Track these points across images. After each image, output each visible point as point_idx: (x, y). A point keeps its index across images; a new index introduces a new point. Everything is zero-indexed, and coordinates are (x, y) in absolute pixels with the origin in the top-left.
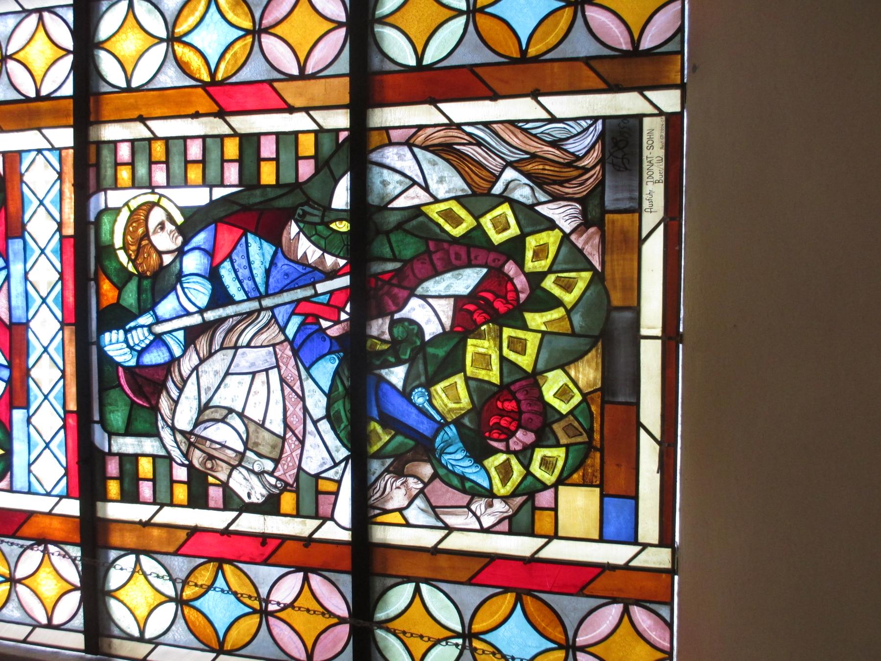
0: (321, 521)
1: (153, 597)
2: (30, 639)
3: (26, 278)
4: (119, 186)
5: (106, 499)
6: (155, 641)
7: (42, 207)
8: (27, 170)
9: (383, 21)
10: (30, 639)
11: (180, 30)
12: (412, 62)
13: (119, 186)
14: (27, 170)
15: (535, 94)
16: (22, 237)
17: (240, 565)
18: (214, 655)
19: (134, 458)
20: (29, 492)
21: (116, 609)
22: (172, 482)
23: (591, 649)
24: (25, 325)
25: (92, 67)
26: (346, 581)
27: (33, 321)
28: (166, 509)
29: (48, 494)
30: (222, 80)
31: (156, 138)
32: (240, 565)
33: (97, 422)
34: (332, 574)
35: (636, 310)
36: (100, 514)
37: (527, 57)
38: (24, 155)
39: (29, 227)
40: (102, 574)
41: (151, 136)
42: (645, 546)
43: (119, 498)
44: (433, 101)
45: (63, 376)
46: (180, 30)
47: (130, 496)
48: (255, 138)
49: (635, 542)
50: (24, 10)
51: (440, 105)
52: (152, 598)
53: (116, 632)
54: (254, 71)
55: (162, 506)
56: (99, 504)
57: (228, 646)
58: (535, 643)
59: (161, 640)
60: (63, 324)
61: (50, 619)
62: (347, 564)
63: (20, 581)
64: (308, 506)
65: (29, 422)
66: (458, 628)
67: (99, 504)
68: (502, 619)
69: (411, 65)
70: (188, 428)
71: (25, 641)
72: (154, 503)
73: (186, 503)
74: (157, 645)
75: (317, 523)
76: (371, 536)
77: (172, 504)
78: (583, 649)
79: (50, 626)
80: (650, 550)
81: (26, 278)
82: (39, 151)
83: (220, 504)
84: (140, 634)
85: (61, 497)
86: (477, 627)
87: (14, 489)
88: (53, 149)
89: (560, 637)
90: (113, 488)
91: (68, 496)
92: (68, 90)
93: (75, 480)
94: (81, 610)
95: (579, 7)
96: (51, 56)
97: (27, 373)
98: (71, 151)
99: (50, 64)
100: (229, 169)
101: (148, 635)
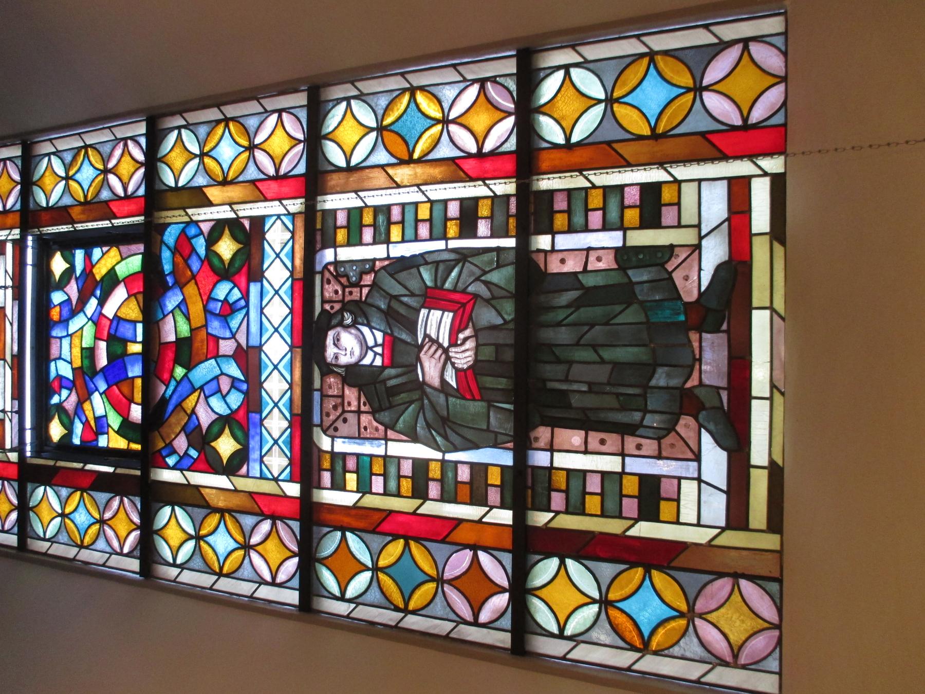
0: (361, 494)
1: (217, 543)
2: (214, 587)
3: (262, 313)
4: (419, 239)
5: (320, 487)
6: (355, 601)
7: (278, 259)
10: (214, 587)
11: (246, 154)
13: (419, 239)
16: (261, 282)
17: (287, 521)
18: (217, 577)
22: (567, 491)
24: (259, 348)
25: (320, 153)
26: (507, 558)
27: (266, 345)
31: (594, 187)
32: (287, 521)
33: (317, 426)
34: (364, 534)
39: (266, 274)
41: (590, 185)
43: (410, 495)
46: (246, 154)
47: (339, 485)
50: (117, 139)
52: (182, 536)
53: (31, 534)
54: (697, 123)
56: (315, 491)
59: (186, 566)
60: (292, 347)
61: (274, 577)
62: (508, 544)
67: (315, 491)
68: (631, 591)
70: (10, 410)
71: (104, 565)
72: (357, 491)
73: (499, 505)
77: (371, 493)
79: (273, 583)
81: (262, 313)
82: (279, 216)
84: (474, 619)
86: (611, 596)
87: (681, 521)
90: (326, 477)
92: (141, 192)
93: (298, 470)
94: (298, 573)
97: (260, 385)
100: (562, 225)
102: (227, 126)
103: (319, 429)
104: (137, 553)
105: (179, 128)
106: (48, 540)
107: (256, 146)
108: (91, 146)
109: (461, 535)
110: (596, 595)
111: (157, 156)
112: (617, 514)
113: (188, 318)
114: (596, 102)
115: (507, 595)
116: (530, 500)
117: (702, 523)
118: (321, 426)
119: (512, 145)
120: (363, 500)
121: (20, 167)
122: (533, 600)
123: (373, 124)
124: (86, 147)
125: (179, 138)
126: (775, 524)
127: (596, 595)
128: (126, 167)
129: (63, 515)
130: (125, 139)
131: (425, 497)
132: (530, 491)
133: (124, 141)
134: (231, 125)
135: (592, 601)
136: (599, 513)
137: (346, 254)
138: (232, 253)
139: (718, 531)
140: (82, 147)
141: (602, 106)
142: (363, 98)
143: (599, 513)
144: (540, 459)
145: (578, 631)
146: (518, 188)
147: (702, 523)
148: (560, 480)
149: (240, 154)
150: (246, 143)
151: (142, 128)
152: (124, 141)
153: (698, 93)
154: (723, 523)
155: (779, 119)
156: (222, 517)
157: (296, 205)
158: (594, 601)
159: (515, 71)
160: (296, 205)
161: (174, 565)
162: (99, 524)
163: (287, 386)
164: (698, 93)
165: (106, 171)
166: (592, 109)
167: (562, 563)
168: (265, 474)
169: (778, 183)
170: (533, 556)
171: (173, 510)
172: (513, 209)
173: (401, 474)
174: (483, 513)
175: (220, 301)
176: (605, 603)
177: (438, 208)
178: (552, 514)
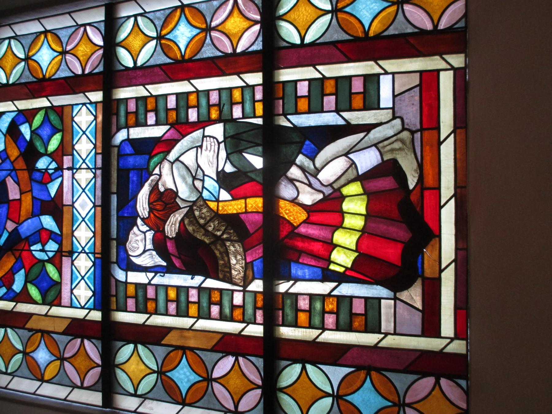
2: (68, 398)
8: (76, 115)
9: (281, 18)
10: (68, 398)
12: (298, 41)
14: (76, 115)
15: (238, 74)
19: (377, 301)
20: (71, 307)
21: (121, 376)
23: (415, 406)
26: (260, 362)
27: (76, 203)
28: (250, 325)
29: (83, 308)
30: (188, 59)
35: (438, 188)
36: (277, 335)
37: (305, 43)
38: (74, 107)
40: (114, 355)
42: (386, 334)
44: (188, 79)
45: (94, 236)
48: (125, 101)
49: (380, 332)
50: (77, 25)
51: (192, 81)
54: (63, 73)
55: (248, 324)
57: (46, 378)
58: (380, 402)
63: (66, 359)
64: (317, 321)
65: (72, 264)
66: (156, 369)
69: (297, 43)
74: (14, 376)
75: (147, 316)
76: (275, 332)
78: (410, 405)
80: (389, 336)
82: (84, 104)
83: (174, 313)
85: (90, 310)
88: (91, 103)
89: (205, 375)
91: (95, 309)
95: (208, 32)
96: (357, 5)
98: (261, 88)
99: (16, 64)
101: (139, 393)
102: (46, 37)
103: (116, 265)
104: (100, 385)
105: (10, 38)
106: (10, 374)
107: (68, 52)
108: (49, 31)
109: (170, 339)
110: (155, 368)
111: (275, 14)
112: (294, 324)
113: (18, 183)
114: (99, 48)
115: (259, 392)
116: (281, 319)
117: (397, 332)
118: (117, 263)
119: (258, 46)
120: (89, 315)
121: (103, 32)
122: (282, 397)
123: (154, 34)
124: (46, 32)
125: (136, 25)
126: (460, 334)
127: (155, 368)
128: (83, 50)
129: (62, 359)
130: (85, 25)
131: (324, 329)
132: (114, 299)
133: (84, 27)
134: (187, 11)
135: (119, 366)
136: (134, 310)
137: (137, 133)
138: (203, 120)
139: (449, 340)
140: (41, 33)
141: (329, 16)
142: (147, 15)
143: (134, 310)
144: (283, 287)
145: (144, 393)
146: (104, 96)
147: (397, 332)
148: (131, 290)
149: (95, 52)
150: (60, 49)
151: (99, 16)
152: (84, 27)
153: (400, 6)
154: (452, 335)
155: (462, 24)
156: (184, 353)
157: (97, 96)
158: (154, 372)
159: (103, 19)
160: (97, 96)
161: (135, 395)
162: (59, 361)
163: (92, 235)
164: (400, 6)
165: (64, 53)
166: (321, 18)
167: (136, 348)
168: (75, 304)
169: (458, 72)
170: (283, 361)
171: (82, 342)
172: (259, 96)
173: (354, 311)
174: (317, 334)
175: (65, 169)
176: (25, 354)
177: (224, 95)
178: (383, 336)
